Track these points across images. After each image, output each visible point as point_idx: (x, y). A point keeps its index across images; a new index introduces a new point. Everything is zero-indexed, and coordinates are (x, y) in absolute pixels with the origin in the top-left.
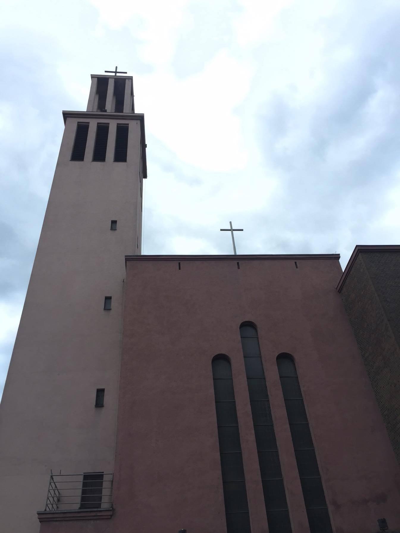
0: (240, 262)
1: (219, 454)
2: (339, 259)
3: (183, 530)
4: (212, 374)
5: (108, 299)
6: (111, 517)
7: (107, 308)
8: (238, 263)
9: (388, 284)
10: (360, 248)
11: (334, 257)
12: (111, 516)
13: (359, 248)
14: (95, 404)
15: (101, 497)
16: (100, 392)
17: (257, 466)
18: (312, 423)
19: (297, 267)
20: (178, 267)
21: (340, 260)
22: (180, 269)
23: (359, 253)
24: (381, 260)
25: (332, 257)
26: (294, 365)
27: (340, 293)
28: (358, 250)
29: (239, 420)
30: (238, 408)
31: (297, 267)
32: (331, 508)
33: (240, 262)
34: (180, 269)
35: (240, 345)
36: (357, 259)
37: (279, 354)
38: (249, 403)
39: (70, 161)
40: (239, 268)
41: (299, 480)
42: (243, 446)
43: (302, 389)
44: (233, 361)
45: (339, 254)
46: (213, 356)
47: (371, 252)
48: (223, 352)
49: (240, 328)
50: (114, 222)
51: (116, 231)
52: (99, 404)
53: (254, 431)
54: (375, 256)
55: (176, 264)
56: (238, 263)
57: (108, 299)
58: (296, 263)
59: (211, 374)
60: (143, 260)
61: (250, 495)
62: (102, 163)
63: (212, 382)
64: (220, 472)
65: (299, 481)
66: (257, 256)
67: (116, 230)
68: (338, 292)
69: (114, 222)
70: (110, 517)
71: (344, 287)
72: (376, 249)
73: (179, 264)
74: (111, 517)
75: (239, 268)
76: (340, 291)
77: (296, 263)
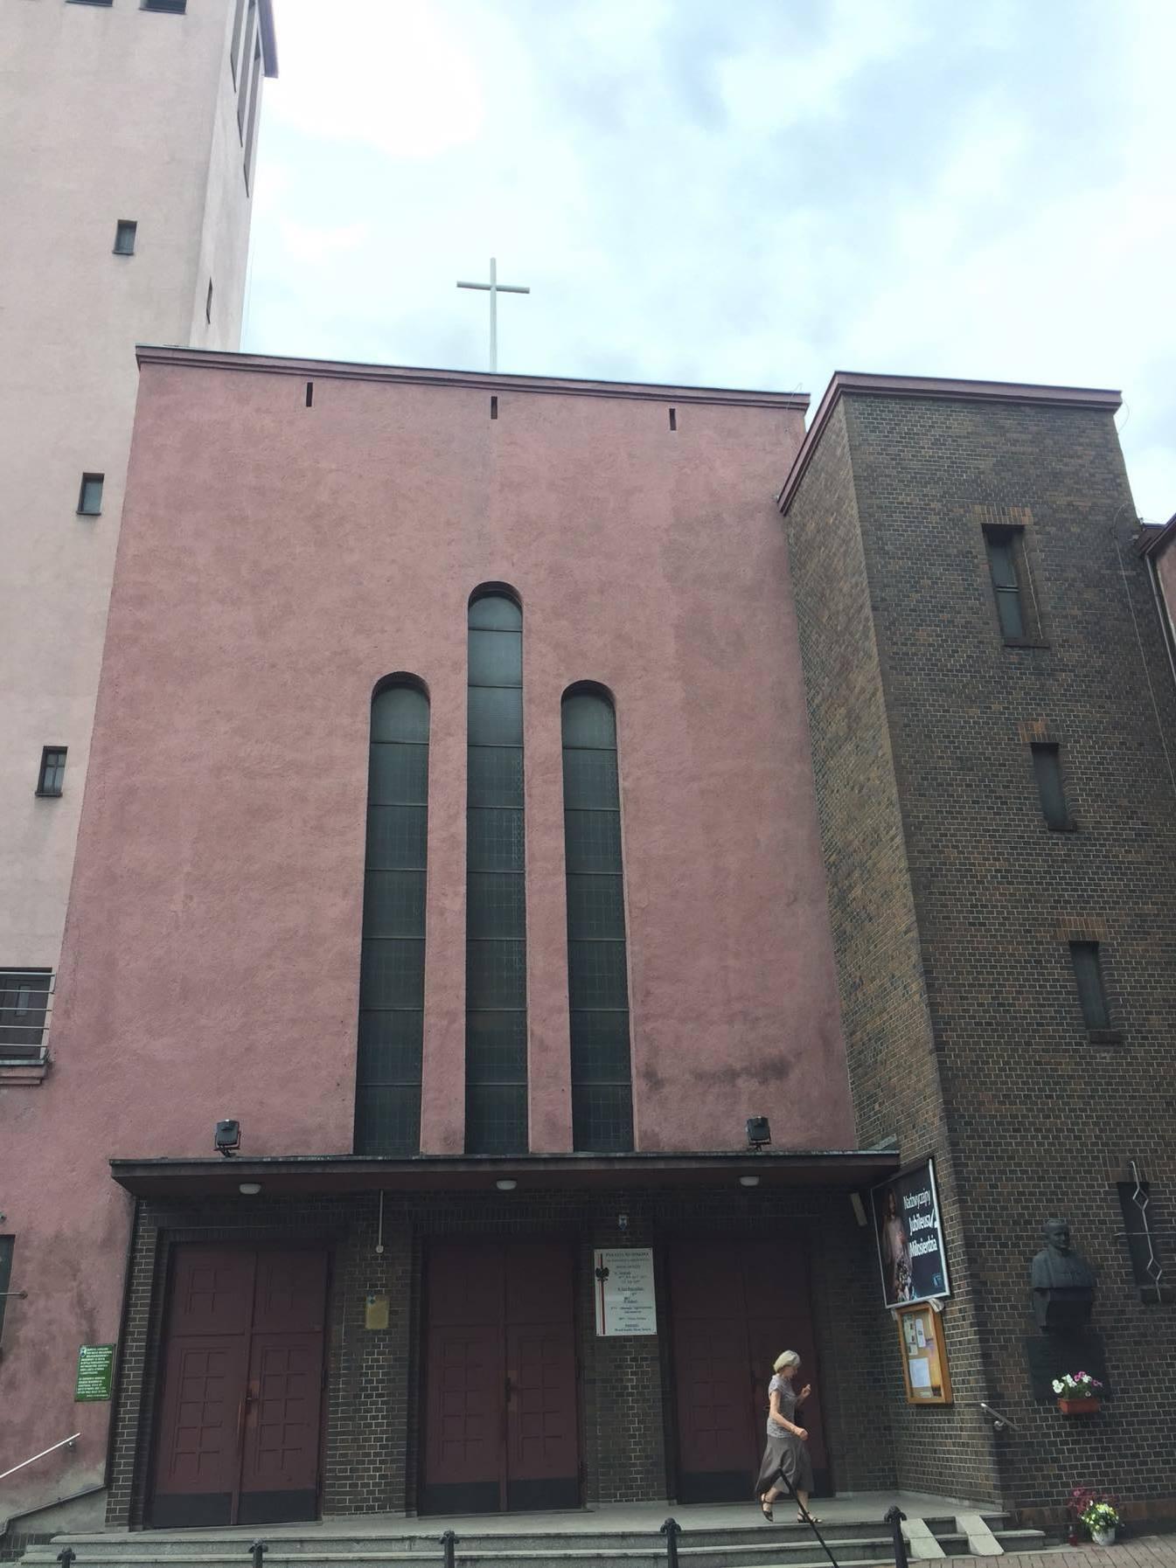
0: (502, 397)
1: (359, 939)
2: (1114, 411)
3: (227, 1120)
4: (367, 728)
5: (92, 480)
6: (41, 1082)
7: (87, 509)
8: (494, 400)
9: (900, 500)
10: (844, 380)
11: (791, 403)
12: (42, 1079)
13: (841, 382)
14: (36, 789)
15: (42, 1031)
16: (53, 756)
17: (458, 974)
18: (630, 874)
19: (673, 427)
20: (304, 399)
21: (1119, 418)
22: (309, 404)
23: (839, 398)
24: (900, 425)
25: (786, 403)
26: (614, 713)
27: (785, 515)
28: (839, 386)
29: (431, 856)
30: (433, 823)
31: (673, 427)
32: (638, 1085)
33: (502, 397)
34: (309, 404)
35: (462, 652)
36: (835, 414)
37: (571, 683)
38: (464, 814)
39: (141, 9)
40: (494, 416)
41: (567, 1015)
42: (432, 921)
43: (622, 784)
44: (435, 695)
45: (1102, 406)
46: (378, 678)
47: (876, 396)
48: (410, 668)
49: (470, 605)
50: (126, 228)
51: (131, 257)
52: (47, 791)
53: (465, 887)
54: (884, 411)
55: (297, 386)
56: (494, 400)
57: (92, 480)
58: (672, 412)
59: (366, 729)
60: (179, 363)
61: (430, 1046)
62: (175, 18)
63: (364, 749)
64: (355, 987)
65: (565, 1018)
66: (557, 382)
67: (132, 254)
68: (782, 511)
69: (126, 228)
70: (38, 1082)
71: (795, 498)
72: (433, 376)
73: (310, 386)
74: (41, 1082)
75: (494, 416)
76: (785, 510)
77: (672, 412)
